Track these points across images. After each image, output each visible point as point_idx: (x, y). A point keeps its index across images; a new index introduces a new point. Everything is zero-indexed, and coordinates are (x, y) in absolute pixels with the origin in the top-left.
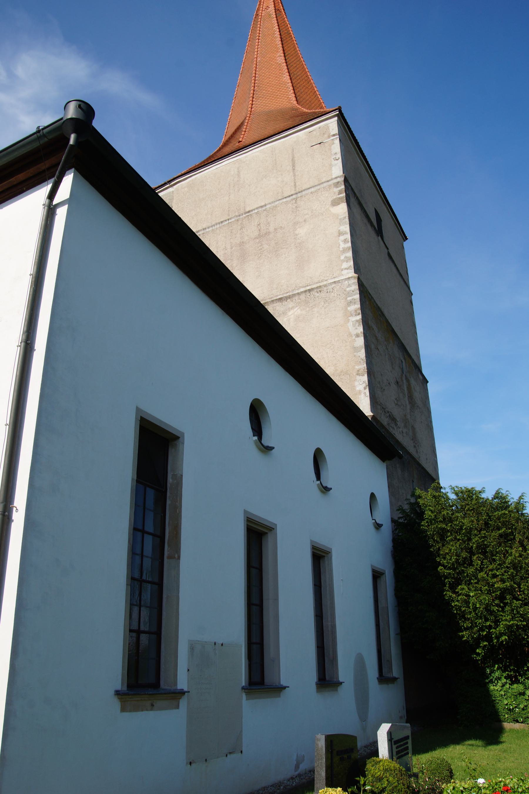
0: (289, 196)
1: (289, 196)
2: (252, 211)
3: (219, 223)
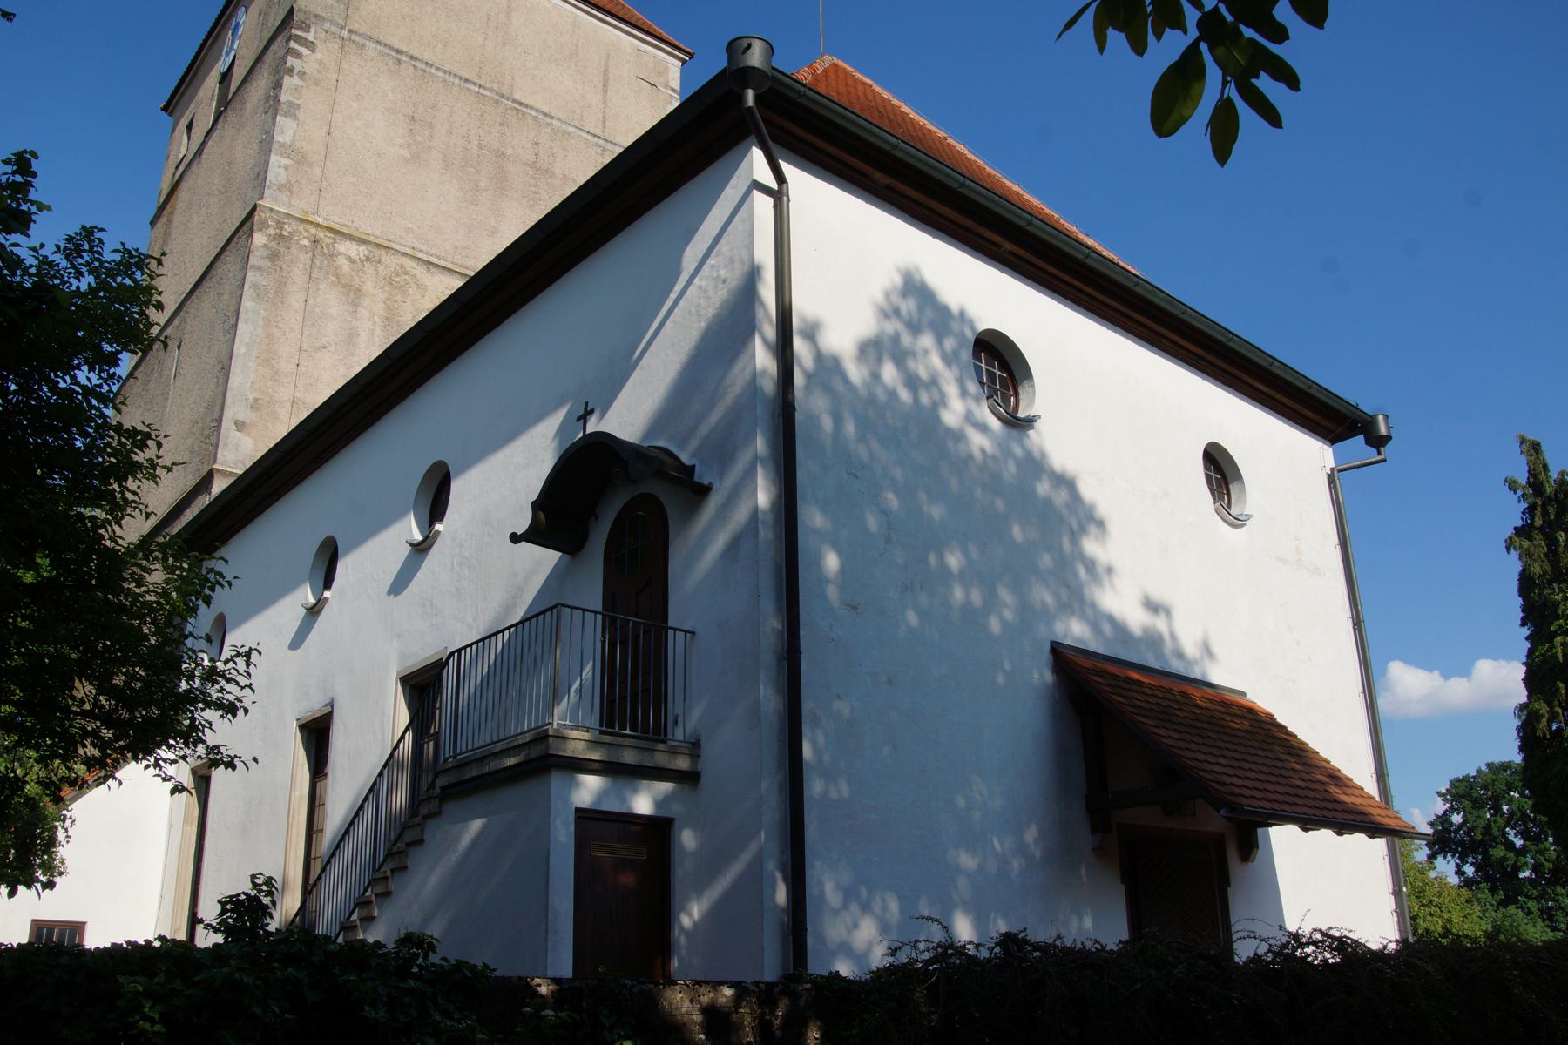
0: (595, 136)
1: (595, 136)
2: (527, 106)
3: (461, 78)
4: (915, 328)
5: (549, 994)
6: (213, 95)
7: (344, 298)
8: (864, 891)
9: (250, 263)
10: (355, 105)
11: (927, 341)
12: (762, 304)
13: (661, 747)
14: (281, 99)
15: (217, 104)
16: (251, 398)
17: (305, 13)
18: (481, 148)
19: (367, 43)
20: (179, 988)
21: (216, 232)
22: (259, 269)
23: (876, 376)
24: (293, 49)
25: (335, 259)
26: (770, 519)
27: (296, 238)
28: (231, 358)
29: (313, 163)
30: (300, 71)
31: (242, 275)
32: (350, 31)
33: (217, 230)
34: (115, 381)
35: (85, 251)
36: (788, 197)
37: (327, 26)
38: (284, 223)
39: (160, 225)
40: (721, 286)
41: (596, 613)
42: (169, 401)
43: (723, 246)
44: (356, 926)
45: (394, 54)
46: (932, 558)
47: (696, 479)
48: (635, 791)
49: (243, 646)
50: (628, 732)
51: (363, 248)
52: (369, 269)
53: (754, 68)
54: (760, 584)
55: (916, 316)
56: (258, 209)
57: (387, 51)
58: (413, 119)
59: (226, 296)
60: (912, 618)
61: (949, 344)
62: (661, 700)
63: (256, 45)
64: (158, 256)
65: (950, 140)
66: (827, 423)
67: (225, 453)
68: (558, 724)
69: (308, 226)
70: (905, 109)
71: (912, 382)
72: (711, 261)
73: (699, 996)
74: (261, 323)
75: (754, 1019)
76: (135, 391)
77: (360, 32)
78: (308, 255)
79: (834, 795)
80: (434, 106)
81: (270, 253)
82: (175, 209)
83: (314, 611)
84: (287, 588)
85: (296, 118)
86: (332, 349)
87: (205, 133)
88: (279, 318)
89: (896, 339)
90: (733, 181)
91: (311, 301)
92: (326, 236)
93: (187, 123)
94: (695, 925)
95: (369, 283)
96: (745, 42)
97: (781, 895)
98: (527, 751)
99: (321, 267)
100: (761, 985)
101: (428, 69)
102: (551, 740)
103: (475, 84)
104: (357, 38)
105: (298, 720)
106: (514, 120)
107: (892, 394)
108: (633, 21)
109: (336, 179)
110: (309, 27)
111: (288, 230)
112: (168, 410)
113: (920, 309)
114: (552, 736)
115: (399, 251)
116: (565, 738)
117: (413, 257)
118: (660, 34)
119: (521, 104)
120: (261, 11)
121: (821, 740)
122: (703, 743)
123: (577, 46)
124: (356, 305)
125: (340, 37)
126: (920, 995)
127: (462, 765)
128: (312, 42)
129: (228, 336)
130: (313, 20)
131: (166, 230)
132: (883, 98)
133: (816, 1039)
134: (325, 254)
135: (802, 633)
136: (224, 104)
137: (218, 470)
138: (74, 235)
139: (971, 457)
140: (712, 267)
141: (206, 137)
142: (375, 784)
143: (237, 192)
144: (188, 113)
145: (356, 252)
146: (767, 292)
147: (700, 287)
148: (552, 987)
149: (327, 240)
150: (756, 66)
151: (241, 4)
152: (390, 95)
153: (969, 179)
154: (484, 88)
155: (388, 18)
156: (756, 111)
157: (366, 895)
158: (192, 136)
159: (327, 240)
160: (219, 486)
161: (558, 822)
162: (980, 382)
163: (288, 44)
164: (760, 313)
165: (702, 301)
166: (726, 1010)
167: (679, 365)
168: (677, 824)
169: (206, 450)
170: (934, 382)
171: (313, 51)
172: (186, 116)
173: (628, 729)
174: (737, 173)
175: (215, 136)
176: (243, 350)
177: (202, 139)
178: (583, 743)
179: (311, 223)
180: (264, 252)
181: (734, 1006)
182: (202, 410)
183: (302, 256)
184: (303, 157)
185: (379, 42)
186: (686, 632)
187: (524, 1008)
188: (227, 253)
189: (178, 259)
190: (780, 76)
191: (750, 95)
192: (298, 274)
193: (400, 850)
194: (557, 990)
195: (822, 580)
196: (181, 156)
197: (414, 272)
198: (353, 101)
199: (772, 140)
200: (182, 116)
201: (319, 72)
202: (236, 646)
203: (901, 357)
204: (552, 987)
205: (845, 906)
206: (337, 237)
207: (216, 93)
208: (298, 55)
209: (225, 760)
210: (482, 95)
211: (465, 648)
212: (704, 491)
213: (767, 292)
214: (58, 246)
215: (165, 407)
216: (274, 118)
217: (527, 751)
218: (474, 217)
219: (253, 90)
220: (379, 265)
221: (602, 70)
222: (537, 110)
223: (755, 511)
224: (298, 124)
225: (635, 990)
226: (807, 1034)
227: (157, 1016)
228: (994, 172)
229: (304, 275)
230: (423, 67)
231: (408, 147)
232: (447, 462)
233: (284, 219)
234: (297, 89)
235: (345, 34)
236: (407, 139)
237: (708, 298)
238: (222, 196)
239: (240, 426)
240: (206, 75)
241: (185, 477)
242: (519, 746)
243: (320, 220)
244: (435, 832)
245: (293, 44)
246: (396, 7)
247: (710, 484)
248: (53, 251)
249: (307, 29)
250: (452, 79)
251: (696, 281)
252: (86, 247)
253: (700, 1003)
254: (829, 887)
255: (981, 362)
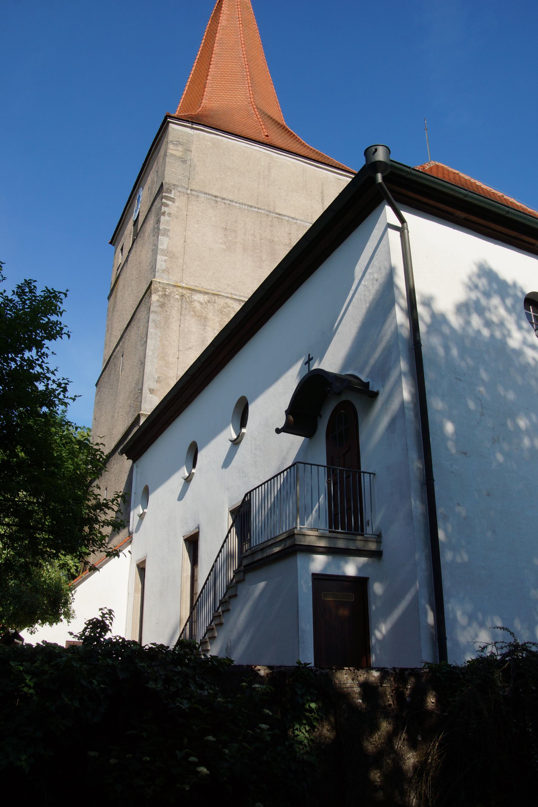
2: (283, 215)
3: (248, 206)
4: (487, 295)
5: (265, 675)
6: (131, 232)
7: (198, 322)
8: (480, 616)
9: (151, 310)
10: (196, 226)
11: (496, 301)
12: (398, 288)
13: (359, 538)
14: (160, 228)
15: (133, 236)
16: (156, 377)
17: (169, 184)
18: (261, 239)
19: (200, 195)
20: (47, 669)
21: (136, 298)
22: (155, 312)
23: (468, 323)
24: (164, 203)
25: (192, 303)
26: (411, 406)
27: (173, 295)
28: (145, 358)
29: (178, 257)
30: (168, 213)
31: (147, 316)
32: (191, 190)
33: (136, 297)
34: (45, 357)
35: (27, 292)
36: (408, 230)
37: (180, 189)
38: (166, 288)
39: (112, 298)
40: (375, 283)
41: (325, 467)
42: (120, 383)
43: (375, 261)
44: (207, 642)
45: (214, 198)
46: (509, 423)
47: (370, 389)
48: (346, 562)
49: (121, 492)
50: (340, 530)
51: (206, 296)
52: (210, 306)
53: (380, 161)
54: (408, 443)
55: (487, 288)
56: (153, 283)
57: (210, 197)
58: (226, 229)
59: (141, 328)
60: (500, 457)
61: (509, 302)
62: (359, 510)
63: (148, 205)
64: (65, 292)
65: (505, 197)
66: (441, 351)
67: (145, 405)
68: (300, 527)
69: (178, 289)
70: (478, 183)
71: (488, 324)
72: (369, 271)
73: (358, 676)
74: (159, 339)
75: (393, 690)
76: (105, 380)
77: (196, 190)
78: (179, 303)
79: (459, 560)
80: (236, 221)
81: (160, 304)
82: (118, 290)
83: (188, 480)
84: (175, 470)
85: (168, 236)
86: (194, 349)
87: (128, 251)
88: (167, 336)
89: (477, 302)
90: (377, 226)
91: (182, 326)
92: (187, 292)
93: (121, 248)
94: (384, 637)
95: (210, 314)
96: (373, 149)
97: (431, 619)
98: (285, 543)
99: (186, 308)
100: (397, 669)
101: (231, 203)
102: (296, 536)
103: (255, 208)
104: (195, 193)
105: (183, 537)
106: (277, 223)
107: (479, 332)
108: (334, 165)
109: (190, 264)
110: (171, 191)
111: (168, 291)
112: (119, 387)
113: (490, 283)
114: (297, 534)
115: (224, 296)
116: (304, 535)
117: (231, 298)
118: (349, 169)
119: (280, 215)
120: (149, 187)
121: (450, 528)
122: (383, 535)
123: (306, 182)
124: (205, 326)
125: (187, 194)
126: (498, 675)
127: (253, 553)
128: (173, 198)
129: (143, 347)
130: (173, 187)
131: (114, 301)
132: (465, 179)
133: (433, 703)
134: (187, 302)
135: (434, 469)
136: (136, 235)
137: (142, 414)
138: (21, 285)
139: (528, 364)
140: (370, 273)
141: (129, 252)
142: (213, 566)
143: (143, 277)
144: (121, 243)
145: (203, 299)
146: (400, 282)
147: (365, 285)
148: (268, 671)
149: (188, 295)
150: (381, 160)
151: (140, 186)
152: (213, 219)
153: (511, 208)
154: (260, 209)
155: (209, 181)
156: (383, 183)
157: (212, 625)
158: (123, 253)
159: (188, 295)
160: (142, 421)
161: (302, 582)
162: (530, 323)
163: (161, 201)
164: (396, 292)
165: (366, 293)
166: (375, 685)
167: (357, 329)
168: (370, 581)
169: (136, 405)
170: (502, 324)
171: (174, 202)
172: (120, 245)
173: (340, 529)
174: (379, 221)
175: (133, 251)
176: (150, 353)
177: (127, 254)
178: (314, 537)
179: (180, 287)
180: (158, 304)
181: (380, 683)
182: (134, 385)
183: (176, 304)
184: (173, 255)
185: (205, 193)
186: (370, 474)
187: (254, 684)
188: (140, 307)
189: (120, 314)
190: (396, 165)
191: (379, 177)
192: (175, 313)
193: (226, 600)
194: (270, 673)
195: (444, 438)
196: (119, 264)
197: (233, 306)
198: (195, 224)
199: (395, 200)
200: (118, 245)
201: (178, 212)
202: (117, 492)
203: (480, 310)
204: (268, 671)
205: (469, 624)
206: (193, 292)
207: (132, 231)
208: (167, 205)
209: (114, 552)
210: (260, 212)
211: (253, 490)
212: (375, 395)
213: (400, 282)
214: (13, 291)
215: (118, 386)
216: (158, 238)
217: (285, 543)
218: (261, 275)
219: (148, 226)
220: (215, 304)
221: (320, 192)
222: (288, 217)
223: (403, 403)
224: (169, 239)
225: (318, 673)
226: (427, 700)
227: (32, 685)
228: (532, 211)
229: (178, 313)
230: (229, 202)
231: (225, 244)
232: (246, 396)
233: (166, 286)
234: (167, 222)
235: (189, 192)
236: (224, 240)
237: (369, 291)
238: (137, 280)
239: (152, 391)
240: (128, 223)
241: (128, 420)
242: (280, 541)
243: (184, 285)
244: (242, 589)
245: (164, 200)
246: (213, 175)
247: (378, 391)
248: (12, 294)
249: (170, 191)
250: (243, 207)
251: (363, 282)
252: (27, 290)
253: (358, 681)
254: (459, 614)
255: (530, 311)
